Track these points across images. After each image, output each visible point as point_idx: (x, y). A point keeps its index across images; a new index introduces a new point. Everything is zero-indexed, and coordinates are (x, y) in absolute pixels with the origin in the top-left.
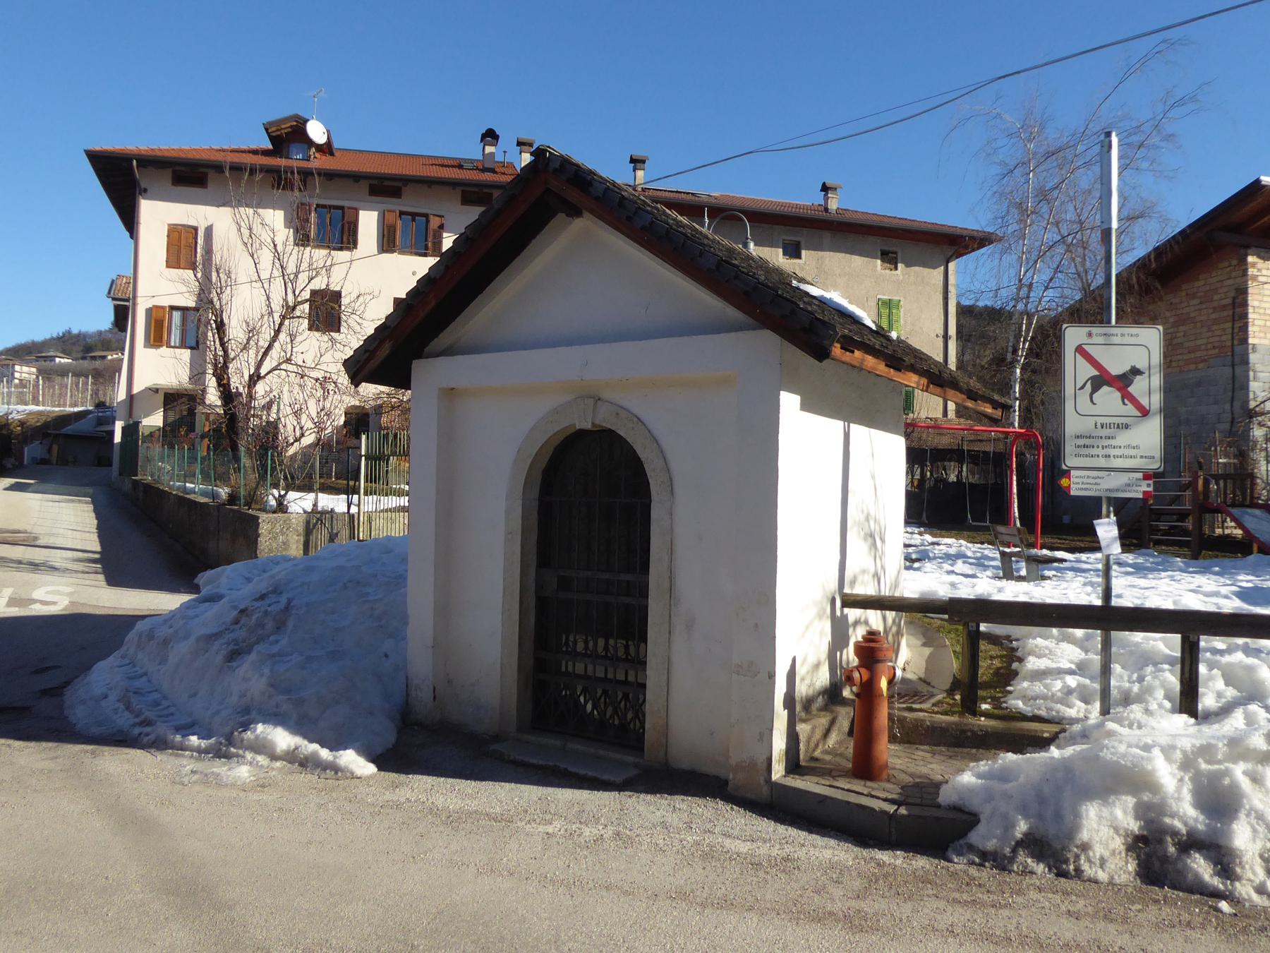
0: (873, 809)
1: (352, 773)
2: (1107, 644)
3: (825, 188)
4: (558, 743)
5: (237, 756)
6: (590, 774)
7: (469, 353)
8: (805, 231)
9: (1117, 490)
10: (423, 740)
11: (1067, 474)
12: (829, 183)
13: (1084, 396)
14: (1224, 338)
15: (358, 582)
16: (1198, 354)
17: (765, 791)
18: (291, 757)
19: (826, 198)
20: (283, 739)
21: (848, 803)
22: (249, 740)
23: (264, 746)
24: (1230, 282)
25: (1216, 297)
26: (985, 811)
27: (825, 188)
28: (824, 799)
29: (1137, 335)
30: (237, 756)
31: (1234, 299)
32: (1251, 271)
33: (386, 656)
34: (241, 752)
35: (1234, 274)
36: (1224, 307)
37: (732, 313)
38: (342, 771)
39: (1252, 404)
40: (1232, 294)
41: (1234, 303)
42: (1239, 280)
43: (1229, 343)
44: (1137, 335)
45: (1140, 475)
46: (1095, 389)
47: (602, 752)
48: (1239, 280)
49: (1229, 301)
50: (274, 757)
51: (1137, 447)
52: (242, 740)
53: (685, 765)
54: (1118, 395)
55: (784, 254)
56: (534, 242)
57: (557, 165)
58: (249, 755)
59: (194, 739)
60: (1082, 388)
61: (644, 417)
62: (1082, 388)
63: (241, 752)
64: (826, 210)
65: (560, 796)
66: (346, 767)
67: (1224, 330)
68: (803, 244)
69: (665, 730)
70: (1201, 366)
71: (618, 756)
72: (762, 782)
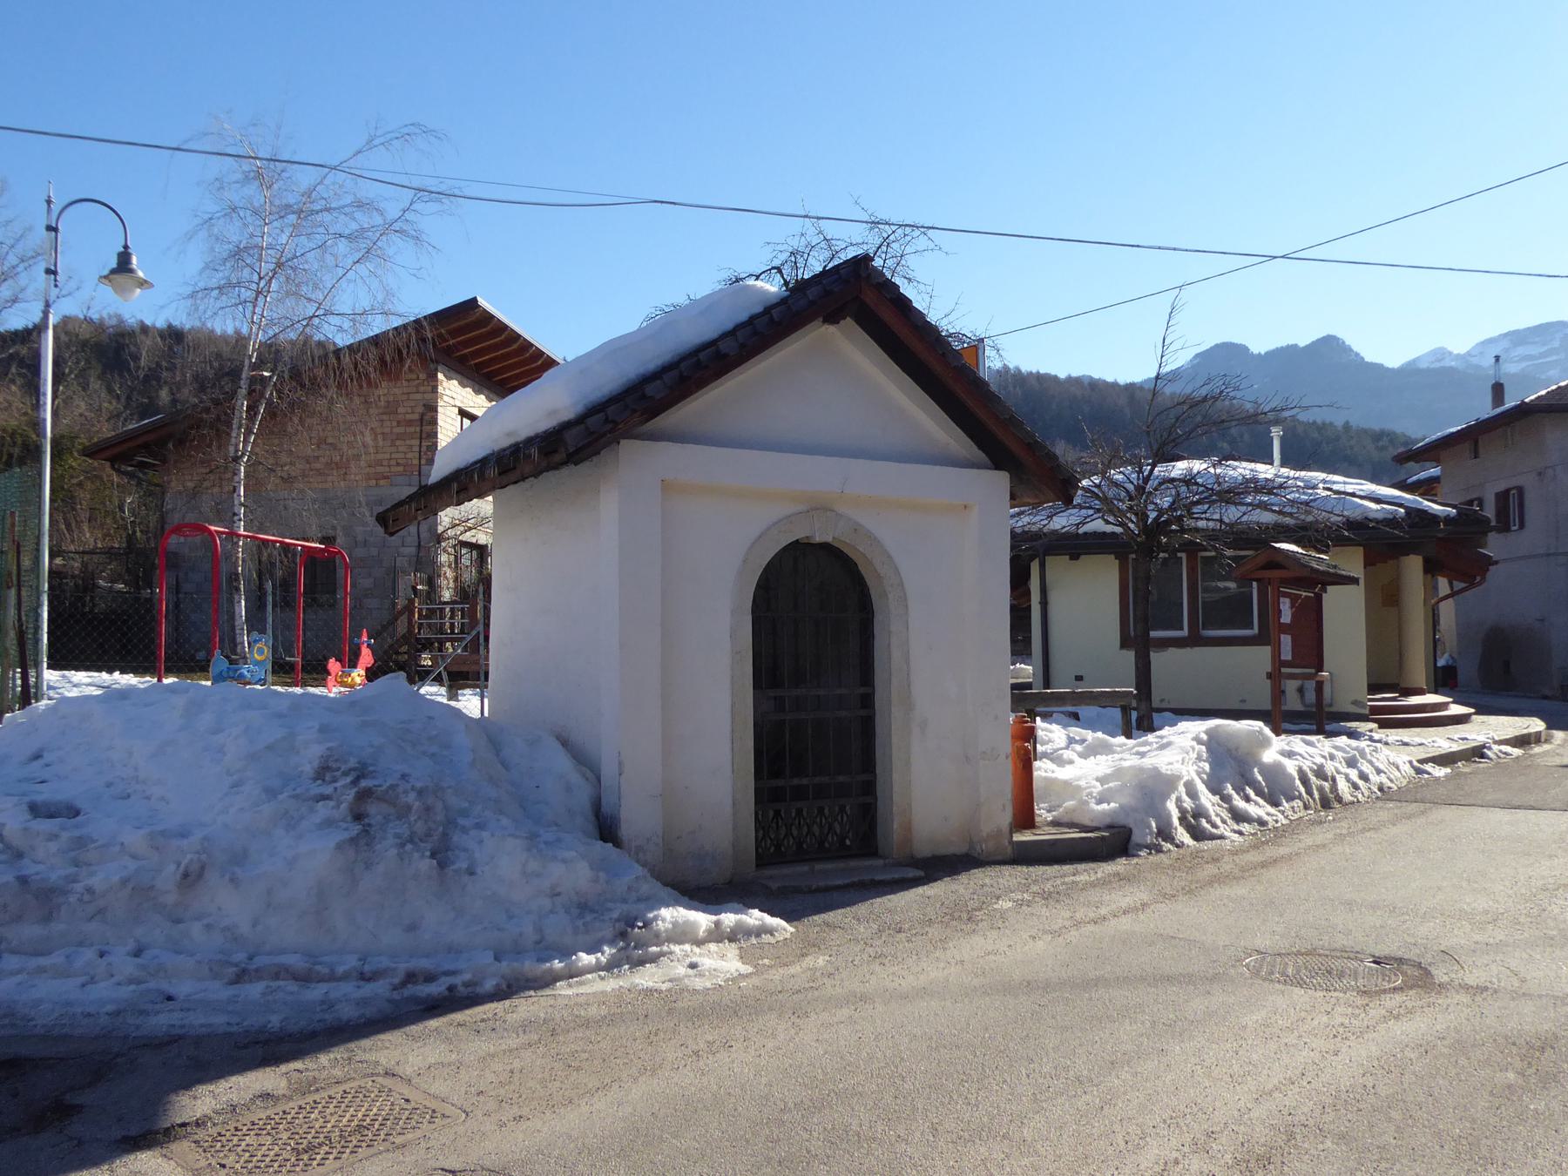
4: (806, 868)
5: (662, 954)
7: (706, 444)
14: (410, 455)
16: (380, 469)
23: (684, 933)
24: (418, 396)
25: (401, 410)
26: (1130, 822)
30: (662, 954)
31: (422, 415)
32: (440, 389)
34: (665, 948)
35: (422, 389)
36: (410, 423)
37: (980, 456)
39: (440, 529)
40: (420, 409)
41: (421, 420)
42: (428, 396)
43: (416, 462)
48: (428, 396)
49: (416, 416)
52: (657, 935)
58: (676, 948)
59: (585, 959)
63: (665, 948)
65: (889, 905)
67: (411, 446)
69: (908, 827)
70: (382, 482)
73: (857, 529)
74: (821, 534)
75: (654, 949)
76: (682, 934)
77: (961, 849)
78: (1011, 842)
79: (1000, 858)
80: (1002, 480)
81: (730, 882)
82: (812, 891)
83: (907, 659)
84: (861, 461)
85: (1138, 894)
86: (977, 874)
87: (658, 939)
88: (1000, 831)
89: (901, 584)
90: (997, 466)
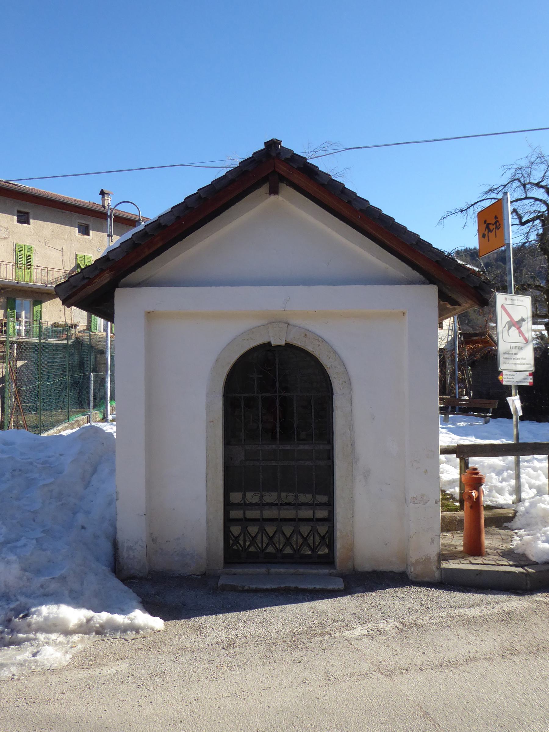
0: (515, 572)
1: (152, 629)
2: (518, 463)
3: (102, 193)
4: (263, 570)
5: (28, 640)
6: (318, 587)
8: (92, 219)
9: (520, 382)
10: (172, 588)
11: (500, 373)
12: (105, 191)
13: (505, 333)
15: (20, 470)
17: (437, 574)
18: (86, 628)
19: (103, 200)
20: (73, 615)
21: (498, 571)
22: (38, 623)
23: (55, 625)
27: (102, 193)
28: (480, 572)
29: (522, 301)
30: (28, 640)
33: (83, 527)
34: (31, 636)
37: (416, 274)
38: (142, 629)
44: (522, 301)
45: (528, 374)
46: (509, 328)
47: (301, 571)
50: (67, 633)
51: (525, 359)
52: (29, 625)
53: (368, 567)
54: (517, 331)
55: (79, 232)
56: (233, 207)
57: (289, 156)
58: (41, 637)
60: (504, 327)
61: (325, 338)
62: (504, 327)
63: (31, 636)
64: (103, 206)
66: (145, 625)
68: (90, 227)
69: (351, 548)
71: (315, 571)
72: (435, 569)
73: (306, 333)
74: (278, 340)
75: (21, 635)
76: (50, 626)
77: (398, 568)
78: (439, 568)
79: (427, 579)
80: (432, 291)
81: (205, 574)
82: (245, 591)
83: (351, 426)
84: (300, 287)
85: (489, 641)
86: (400, 592)
87: (29, 628)
88: (428, 559)
89: (346, 372)
90: (430, 280)
